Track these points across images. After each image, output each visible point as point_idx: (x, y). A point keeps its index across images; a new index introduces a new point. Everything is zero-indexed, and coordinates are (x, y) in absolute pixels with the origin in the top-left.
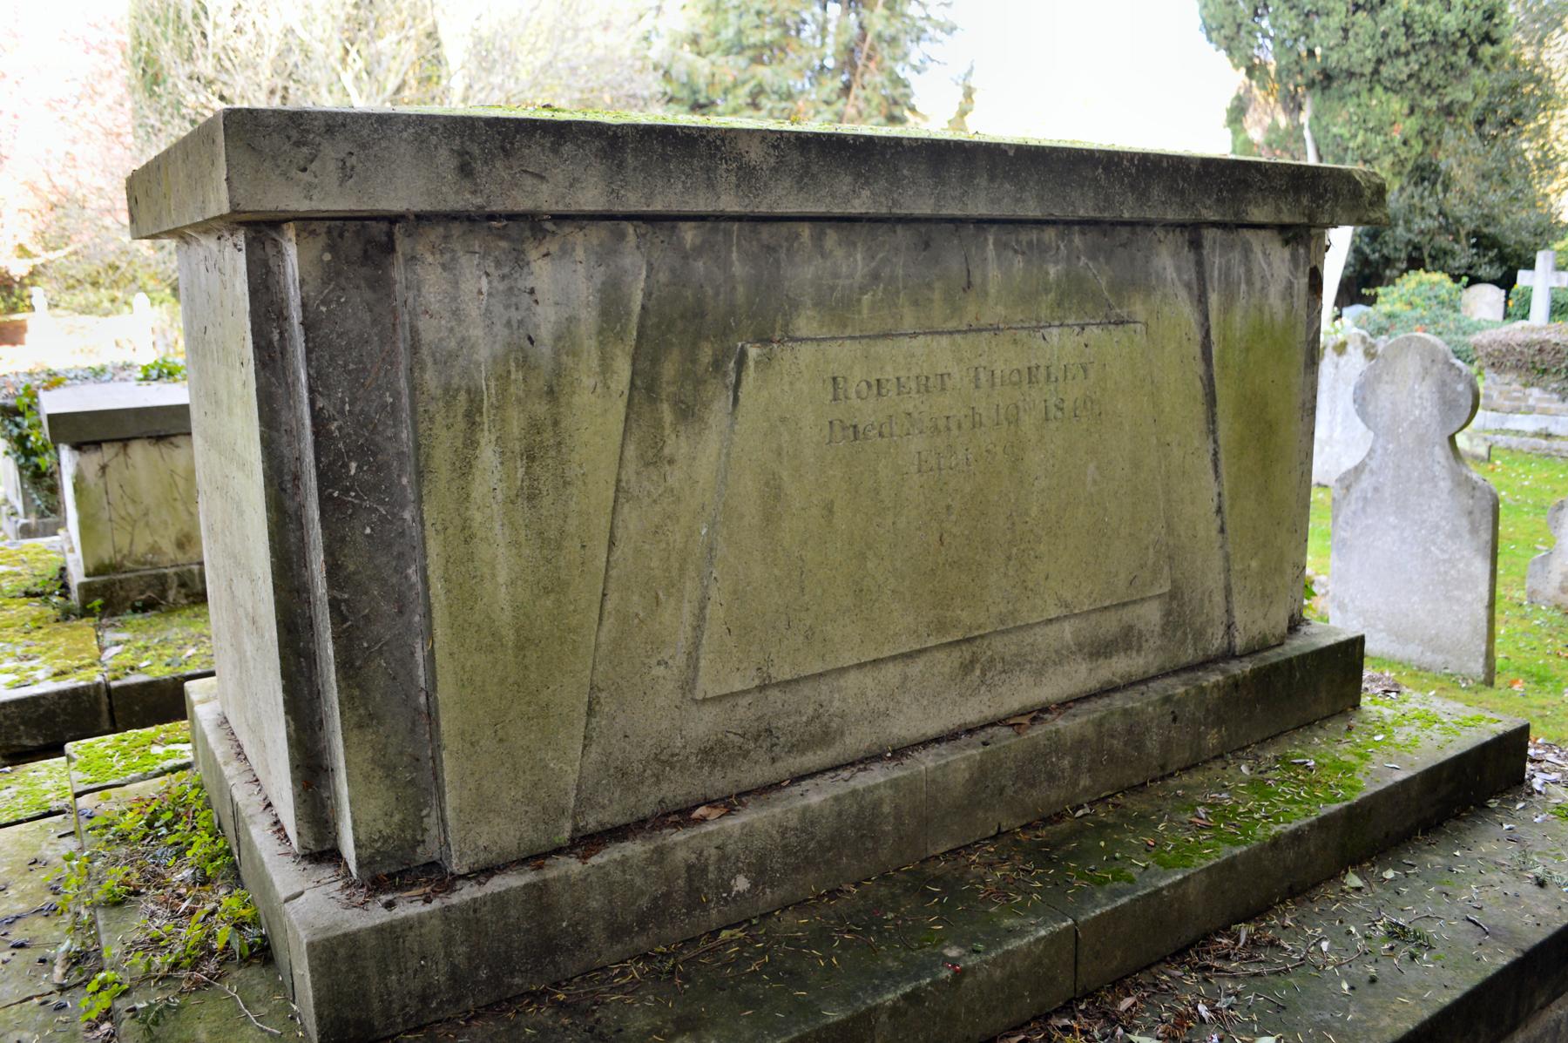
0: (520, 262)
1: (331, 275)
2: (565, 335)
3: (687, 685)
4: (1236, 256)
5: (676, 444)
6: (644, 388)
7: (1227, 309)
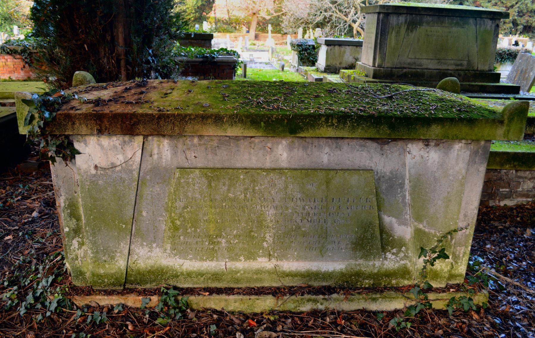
0: (399, 17)
1: (384, 17)
2: (402, 23)
3: (408, 56)
4: (482, 21)
5: (410, 34)
6: (408, 29)
7: (480, 28)
